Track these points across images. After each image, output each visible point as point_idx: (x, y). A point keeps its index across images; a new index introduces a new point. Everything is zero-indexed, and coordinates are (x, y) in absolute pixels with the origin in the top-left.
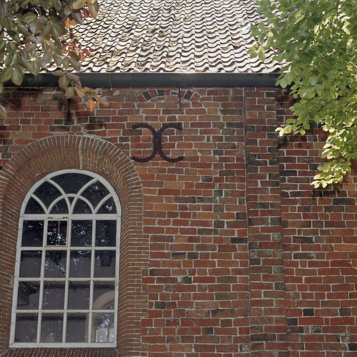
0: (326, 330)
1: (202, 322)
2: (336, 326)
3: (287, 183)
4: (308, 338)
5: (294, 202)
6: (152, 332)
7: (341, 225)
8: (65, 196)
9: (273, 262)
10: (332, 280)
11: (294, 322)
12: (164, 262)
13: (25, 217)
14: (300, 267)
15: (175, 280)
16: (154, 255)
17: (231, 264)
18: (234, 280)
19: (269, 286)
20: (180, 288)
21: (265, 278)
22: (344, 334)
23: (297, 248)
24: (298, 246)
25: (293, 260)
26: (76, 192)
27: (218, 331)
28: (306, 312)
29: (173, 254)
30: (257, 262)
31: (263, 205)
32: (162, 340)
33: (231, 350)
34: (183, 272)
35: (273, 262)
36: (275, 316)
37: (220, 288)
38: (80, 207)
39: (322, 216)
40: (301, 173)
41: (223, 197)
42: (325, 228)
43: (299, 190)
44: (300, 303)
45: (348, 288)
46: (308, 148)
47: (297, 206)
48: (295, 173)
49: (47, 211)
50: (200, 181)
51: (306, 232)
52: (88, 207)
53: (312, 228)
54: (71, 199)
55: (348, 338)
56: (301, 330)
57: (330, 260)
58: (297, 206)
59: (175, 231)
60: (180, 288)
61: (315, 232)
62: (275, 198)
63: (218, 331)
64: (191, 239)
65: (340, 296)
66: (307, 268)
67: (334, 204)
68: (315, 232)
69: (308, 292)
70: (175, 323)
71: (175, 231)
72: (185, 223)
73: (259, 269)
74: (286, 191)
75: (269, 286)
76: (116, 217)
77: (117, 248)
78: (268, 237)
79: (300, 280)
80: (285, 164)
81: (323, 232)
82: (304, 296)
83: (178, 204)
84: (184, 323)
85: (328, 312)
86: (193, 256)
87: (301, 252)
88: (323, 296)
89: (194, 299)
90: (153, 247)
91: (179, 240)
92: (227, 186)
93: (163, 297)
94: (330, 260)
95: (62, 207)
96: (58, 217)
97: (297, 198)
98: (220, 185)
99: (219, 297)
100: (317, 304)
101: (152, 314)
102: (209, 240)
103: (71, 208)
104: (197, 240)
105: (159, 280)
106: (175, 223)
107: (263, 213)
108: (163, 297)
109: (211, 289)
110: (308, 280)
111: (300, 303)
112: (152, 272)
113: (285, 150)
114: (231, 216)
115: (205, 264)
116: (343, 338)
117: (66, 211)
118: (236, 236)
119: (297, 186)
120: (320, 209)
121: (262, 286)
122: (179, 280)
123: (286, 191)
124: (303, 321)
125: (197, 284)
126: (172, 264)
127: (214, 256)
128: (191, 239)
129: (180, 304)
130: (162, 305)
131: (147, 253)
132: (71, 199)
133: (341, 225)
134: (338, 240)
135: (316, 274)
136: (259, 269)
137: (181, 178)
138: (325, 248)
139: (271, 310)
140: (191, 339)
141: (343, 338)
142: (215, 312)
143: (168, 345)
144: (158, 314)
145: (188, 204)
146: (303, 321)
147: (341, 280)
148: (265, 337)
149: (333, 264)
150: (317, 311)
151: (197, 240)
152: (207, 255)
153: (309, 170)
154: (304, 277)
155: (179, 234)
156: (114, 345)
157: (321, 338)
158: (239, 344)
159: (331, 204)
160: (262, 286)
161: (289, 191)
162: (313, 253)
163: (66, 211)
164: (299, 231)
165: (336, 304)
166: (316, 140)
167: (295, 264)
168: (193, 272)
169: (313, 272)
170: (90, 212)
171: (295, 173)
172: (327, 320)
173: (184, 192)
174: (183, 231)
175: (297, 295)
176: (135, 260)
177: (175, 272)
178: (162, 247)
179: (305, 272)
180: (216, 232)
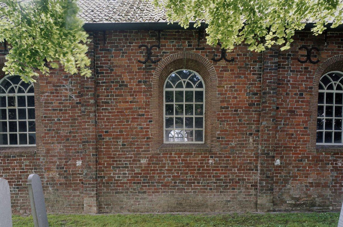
0: (113, 138)
1: (66, 136)
2: (117, 137)
3: (100, 77)
4: (106, 142)
5: (103, 86)
6: (46, 140)
7: (122, 96)
8: (13, 85)
9: (90, 112)
10: (116, 119)
11: (101, 136)
12: (50, 113)
13: (165, 90)
14: (104, 114)
15: (54, 120)
16: (45, 110)
17: (76, 113)
18: (77, 119)
19: (89, 122)
20: (56, 123)
21: (88, 118)
22: (120, 140)
23: (103, 106)
24: (104, 105)
25: (101, 111)
26: (186, 79)
27: (71, 140)
28: (106, 132)
29: (53, 109)
30: (84, 112)
31: (87, 88)
32: (50, 143)
33: (76, 147)
34: (56, 117)
35: (90, 112)
36: (91, 134)
37: (72, 123)
38: (20, 91)
39: (114, 92)
40: (106, 73)
41: (73, 84)
42: (115, 97)
43: (105, 81)
44: (103, 128)
45: (123, 122)
46: (109, 61)
47: (104, 88)
48: (103, 73)
49: (7, 92)
50: (63, 78)
51: (107, 99)
52: (192, 86)
53: (109, 97)
54: (184, 82)
55: (122, 142)
56: (103, 139)
57: (116, 111)
58: (104, 88)
59: (53, 100)
60: (56, 123)
61: (111, 99)
62: (91, 84)
63: (71, 140)
64: (60, 103)
65: (119, 125)
66: (107, 114)
67: (119, 87)
68: (111, 99)
69: (107, 124)
70: (55, 137)
71: (53, 100)
72: (57, 96)
73: (85, 115)
74: (99, 81)
75: (89, 122)
76: (203, 89)
77: (165, 103)
78: (89, 102)
79: (104, 119)
80: (99, 69)
81: (114, 99)
82: (105, 125)
83: (54, 88)
84: (58, 137)
85: (114, 132)
86: (61, 110)
87: (104, 107)
88: (113, 125)
89: (62, 127)
90: (45, 107)
91: (56, 104)
92: (74, 80)
93: (50, 127)
94: (116, 111)
95: (180, 85)
96: (11, 95)
97: (104, 84)
98: (71, 79)
99: (72, 126)
100: (110, 129)
101: (46, 134)
102: (67, 103)
103: (16, 91)
104: (62, 103)
105: (48, 120)
106: (53, 96)
107: (87, 91)
108: (50, 127)
109: (68, 123)
110: (107, 119)
111: (103, 128)
112: (45, 117)
113: (99, 62)
114: (76, 93)
115: (66, 114)
116: (120, 141)
117: (182, 87)
118: (78, 101)
119: (104, 79)
120: (113, 89)
121: (86, 122)
122: (56, 120)
123: (99, 81)
124: (104, 135)
125: (63, 121)
126: (52, 114)
127: (69, 110)
128: (60, 103)
129: (56, 129)
130: (49, 130)
131: (43, 109)
132: (16, 87)
133: (122, 96)
134: (120, 102)
135: (110, 117)
136: (85, 115)
137: (55, 77)
138: (114, 106)
139: (90, 131)
140: (61, 143)
141: (120, 141)
142: (70, 132)
143: (52, 145)
144: (48, 134)
145: (58, 88)
146: (104, 135)
147: (119, 119)
148: (87, 142)
149: (118, 112)
150: (110, 131)
151: (62, 103)
152: (66, 110)
153: (109, 71)
154: (105, 118)
155: (55, 101)
156: (164, 143)
157: (111, 142)
158: (79, 145)
159: (118, 87)
160: (86, 122)
161: (101, 81)
162: (109, 108)
163: (182, 87)
164: (104, 99)
165: (118, 128)
166: (113, 57)
167: (102, 113)
168: (61, 117)
169: (109, 116)
170: (192, 87)
171: (103, 73)
172: (114, 135)
173: (57, 83)
174: (57, 100)
175: (103, 125)
176: (38, 112)
177: (54, 117)
178: (49, 107)
179: (106, 116)
180: (70, 100)
